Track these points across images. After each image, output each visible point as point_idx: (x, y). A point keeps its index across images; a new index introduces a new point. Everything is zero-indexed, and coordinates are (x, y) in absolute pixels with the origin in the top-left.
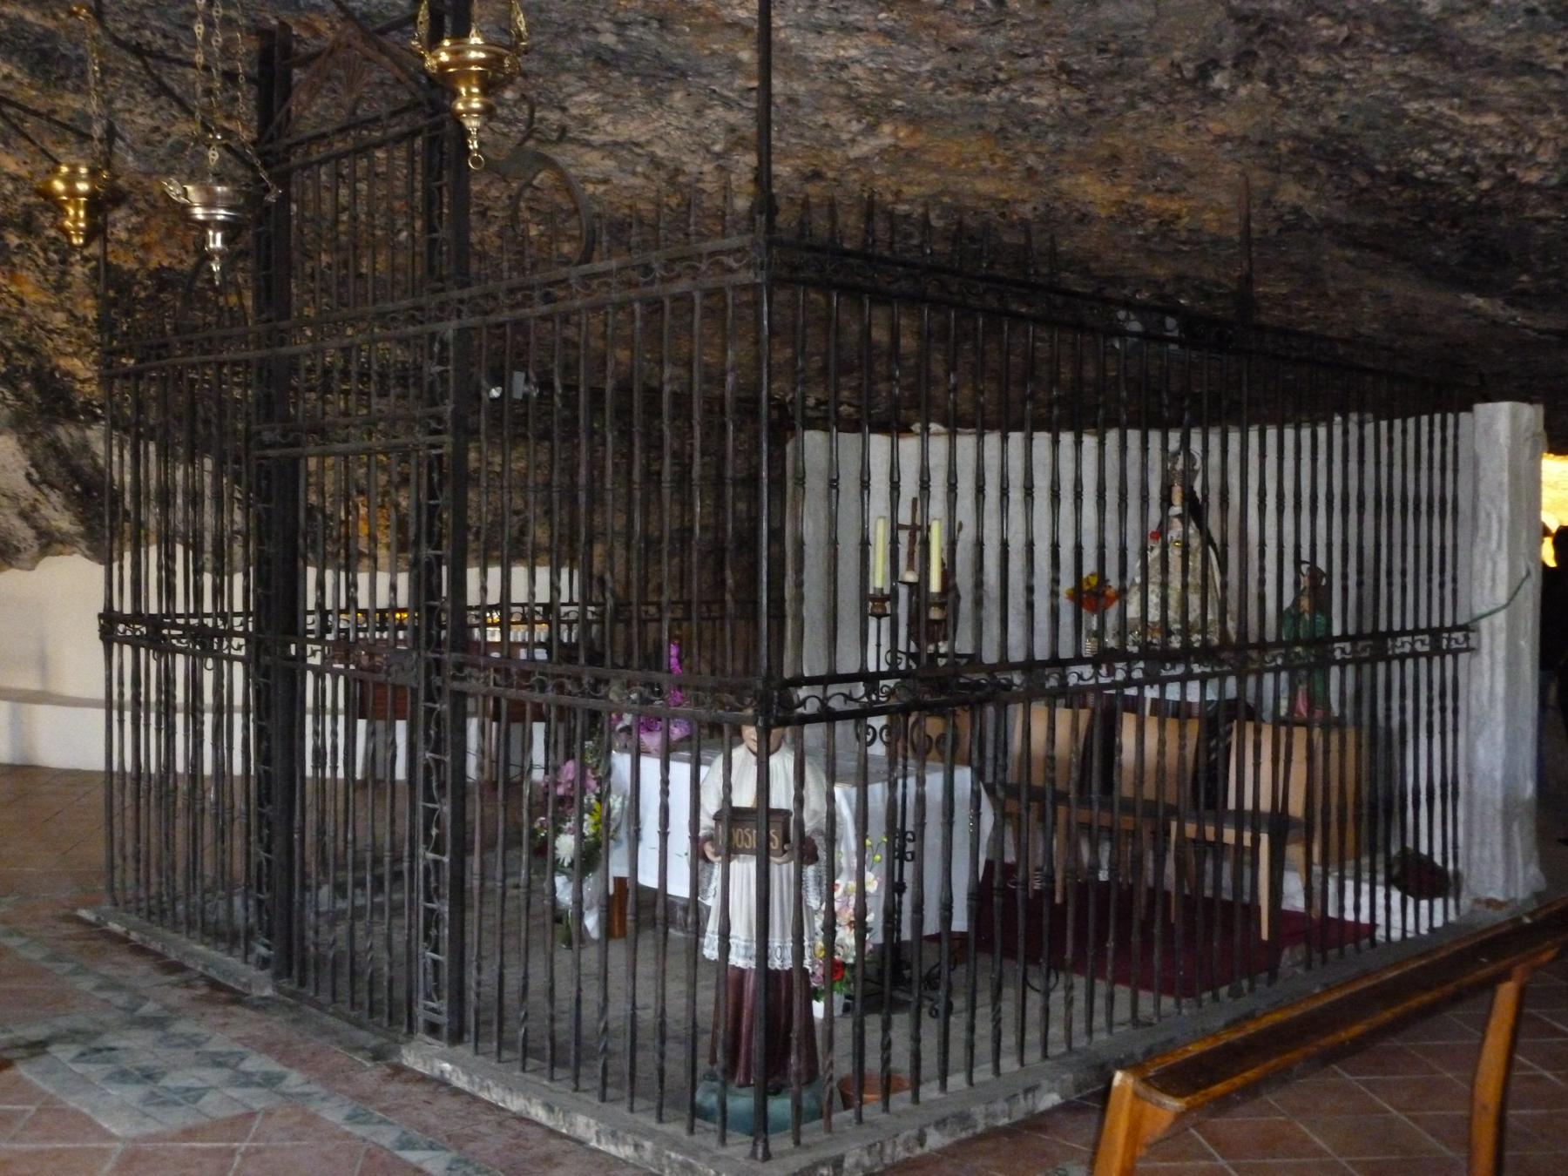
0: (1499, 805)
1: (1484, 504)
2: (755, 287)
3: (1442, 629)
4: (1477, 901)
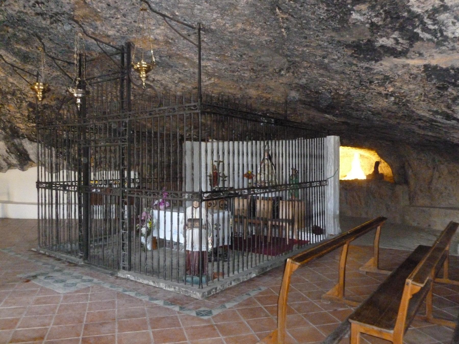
0: (333, 216)
1: (329, 156)
2: (198, 114)
3: (322, 181)
4: (329, 235)
